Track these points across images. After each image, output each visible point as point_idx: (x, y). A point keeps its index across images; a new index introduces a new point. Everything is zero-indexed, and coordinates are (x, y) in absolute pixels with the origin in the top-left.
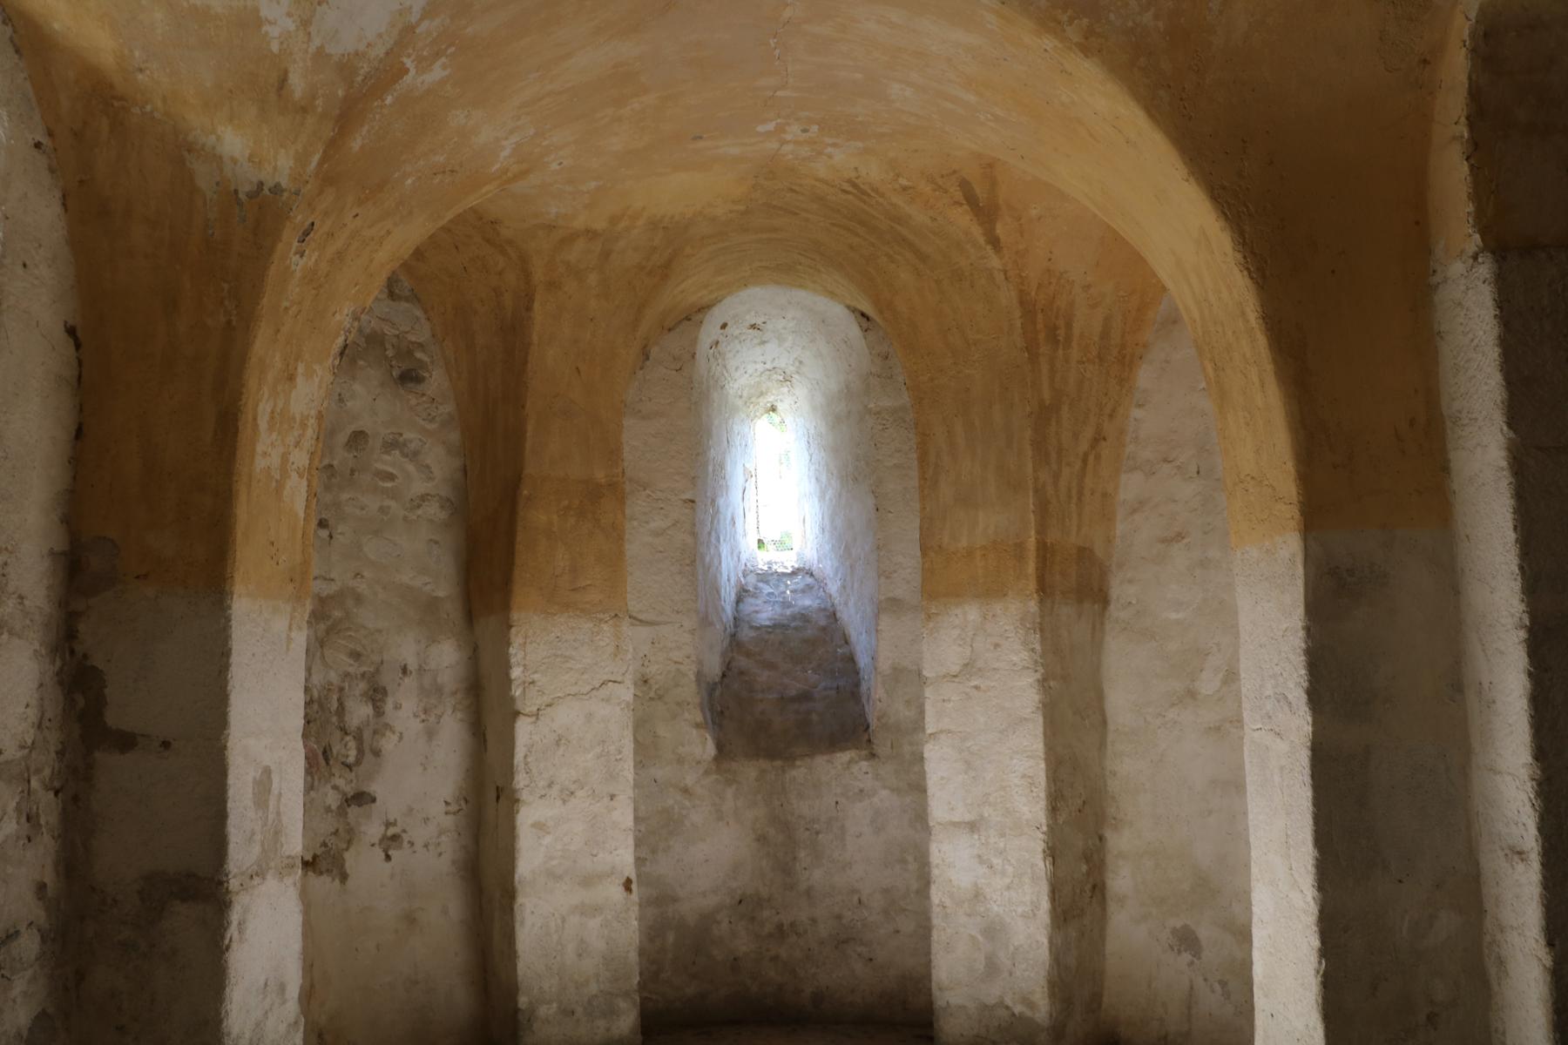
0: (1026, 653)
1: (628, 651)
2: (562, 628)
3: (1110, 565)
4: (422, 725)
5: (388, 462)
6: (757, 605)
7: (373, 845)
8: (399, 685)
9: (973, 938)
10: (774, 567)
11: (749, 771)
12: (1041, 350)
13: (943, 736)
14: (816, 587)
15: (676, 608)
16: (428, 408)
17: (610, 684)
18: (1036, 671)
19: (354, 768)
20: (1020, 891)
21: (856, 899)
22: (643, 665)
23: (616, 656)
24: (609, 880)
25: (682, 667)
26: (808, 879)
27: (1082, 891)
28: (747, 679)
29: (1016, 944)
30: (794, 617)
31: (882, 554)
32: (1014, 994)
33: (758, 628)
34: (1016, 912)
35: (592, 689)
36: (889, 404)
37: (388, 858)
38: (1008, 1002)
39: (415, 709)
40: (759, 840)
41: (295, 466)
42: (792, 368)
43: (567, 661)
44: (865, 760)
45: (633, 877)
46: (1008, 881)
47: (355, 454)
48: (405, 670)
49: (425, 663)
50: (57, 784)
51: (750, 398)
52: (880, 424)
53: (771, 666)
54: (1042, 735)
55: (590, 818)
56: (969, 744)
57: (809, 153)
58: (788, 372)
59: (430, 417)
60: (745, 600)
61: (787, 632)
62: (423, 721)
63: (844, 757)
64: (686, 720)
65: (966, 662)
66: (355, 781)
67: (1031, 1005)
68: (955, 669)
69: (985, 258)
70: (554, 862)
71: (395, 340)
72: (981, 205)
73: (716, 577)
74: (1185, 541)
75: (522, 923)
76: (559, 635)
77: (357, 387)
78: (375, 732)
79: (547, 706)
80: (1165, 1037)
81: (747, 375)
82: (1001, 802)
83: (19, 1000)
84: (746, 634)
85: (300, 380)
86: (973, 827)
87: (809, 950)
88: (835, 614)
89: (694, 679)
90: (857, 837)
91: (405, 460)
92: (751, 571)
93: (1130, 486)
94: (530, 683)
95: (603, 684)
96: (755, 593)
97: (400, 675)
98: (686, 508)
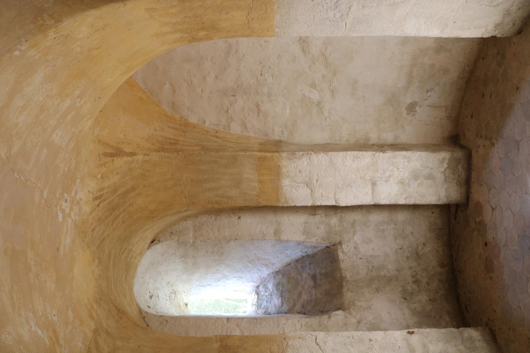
0: (304, 158)
1: (301, 334)
3: (266, 139)
6: (272, 306)
9: (418, 185)
10: (255, 303)
11: (348, 296)
12: (179, 148)
13: (337, 197)
14: (265, 283)
15: (277, 326)
17: (317, 341)
18: (311, 154)
20: (399, 164)
21: (399, 251)
23: (303, 339)
24: (410, 341)
25: (304, 324)
26: (393, 271)
28: (306, 304)
29: (420, 166)
30: (278, 289)
31: (255, 238)
32: (439, 167)
33: (282, 303)
34: (407, 166)
35: (320, 349)
36: (192, 232)
38: (443, 170)
40: (378, 292)
42: (170, 288)
44: (342, 246)
45: (407, 331)
46: (395, 169)
51: (181, 311)
52: (200, 237)
53: (300, 294)
54: (337, 153)
55: (382, 350)
56: (340, 185)
57: (77, 208)
58: (172, 291)
60: (269, 312)
61: (284, 291)
63: (341, 256)
64: (327, 322)
65: (306, 185)
67: (444, 159)
68: (309, 191)
69: (138, 161)
72: (115, 153)
74: (260, 103)
80: (448, 117)
82: (364, 171)
84: (285, 308)
86: (374, 184)
87: (422, 269)
88: (277, 272)
89: (309, 319)
90: (374, 250)
92: (256, 312)
93: (236, 128)
95: (317, 344)
96: (266, 308)
98: (231, 321)
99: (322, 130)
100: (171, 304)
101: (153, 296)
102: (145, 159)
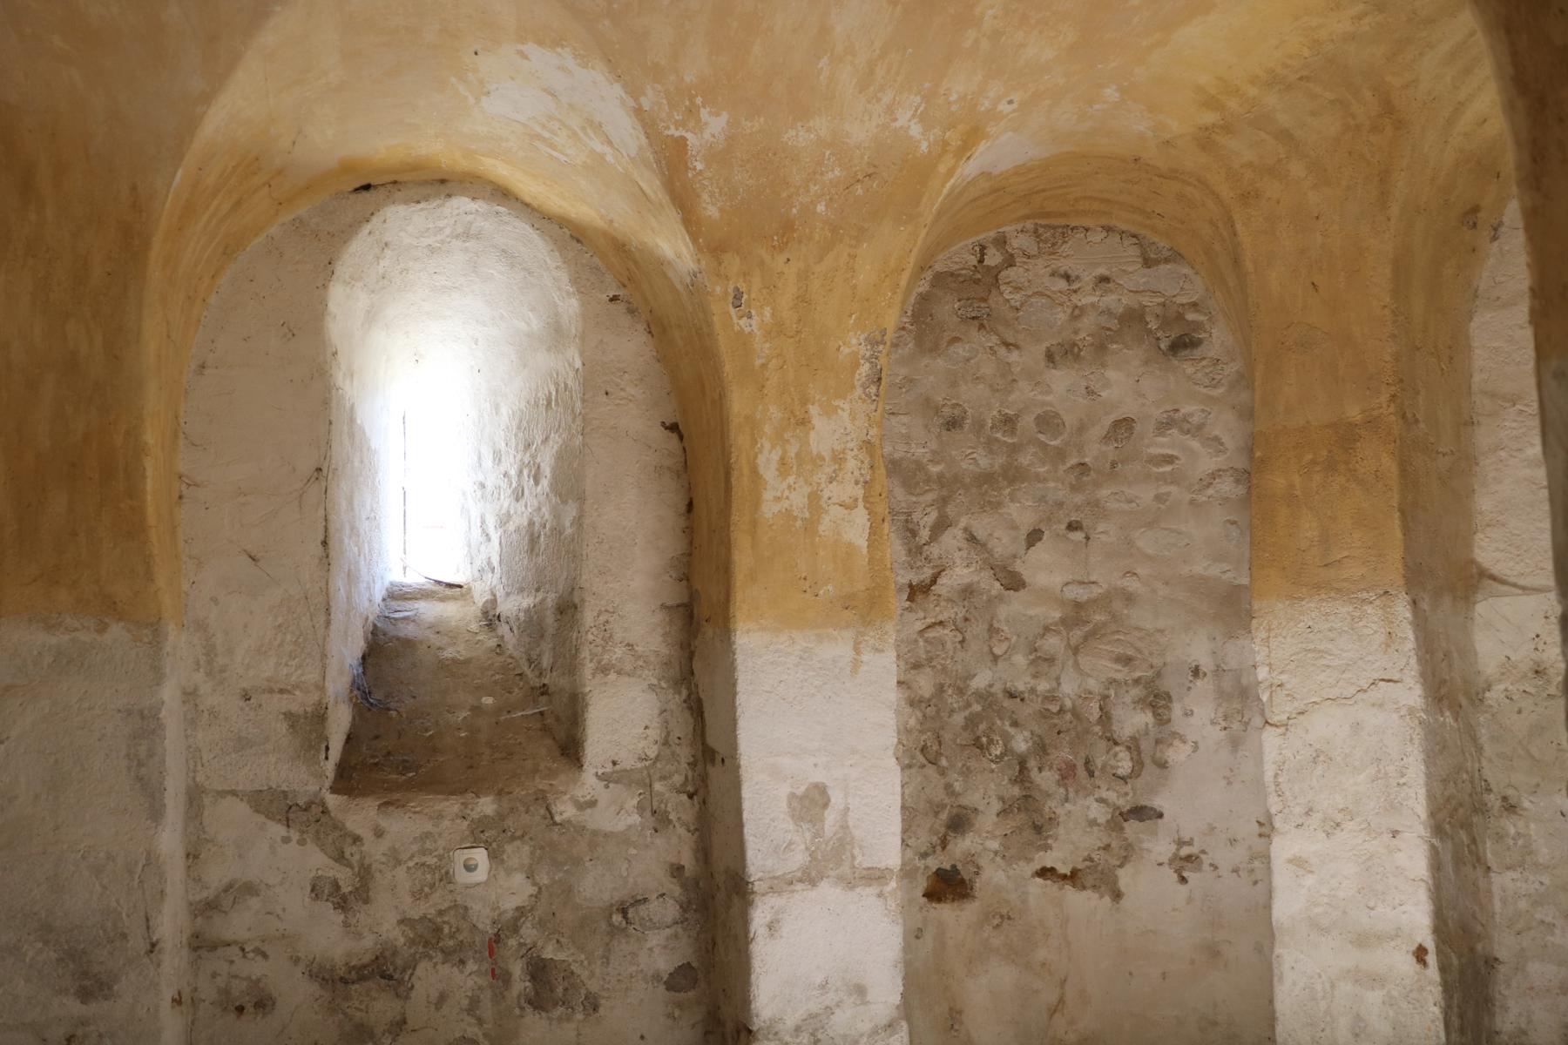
2: (1313, 614)
4: (1224, 733)
5: (1162, 445)
7: (1160, 864)
8: (1189, 689)
16: (1211, 372)
19: (1129, 780)
22: (1536, 649)
23: (1388, 646)
37: (1183, 880)
39: (1213, 716)
43: (1322, 657)
47: (1116, 445)
48: (1196, 672)
49: (1224, 663)
50: (690, 789)
55: (1364, 858)
59: (1215, 382)
62: (1225, 729)
66: (1131, 795)
70: (1319, 910)
71: (1159, 310)
75: (1281, 978)
76: (1311, 624)
77: (1111, 374)
78: (1158, 742)
79: (1299, 713)
83: (657, 951)
94: (1279, 686)
95: (1373, 684)
97: (1191, 678)
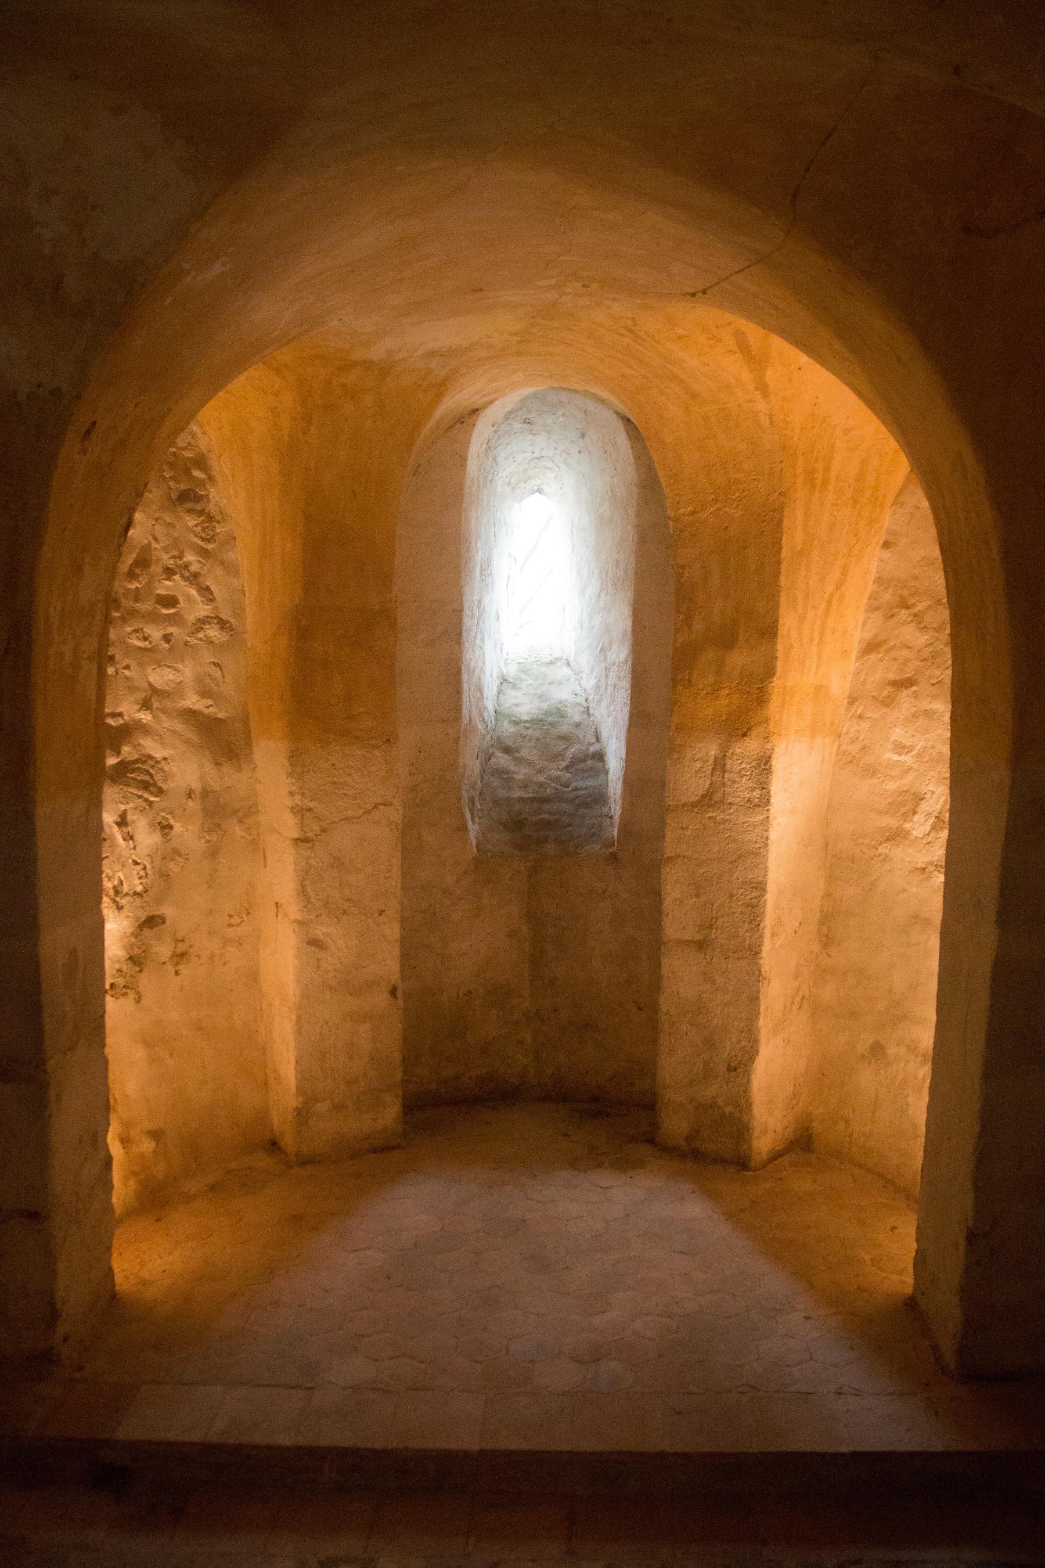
4: (207, 844)
6: (516, 697)
27: (793, 1003)
41: (85, 655)
73: (480, 679)
74: (914, 688)
81: (516, 464)
85: (87, 570)
91: (187, 583)
99: (854, 835)
100: (527, 461)
101: (529, 424)
102: (761, 415)
